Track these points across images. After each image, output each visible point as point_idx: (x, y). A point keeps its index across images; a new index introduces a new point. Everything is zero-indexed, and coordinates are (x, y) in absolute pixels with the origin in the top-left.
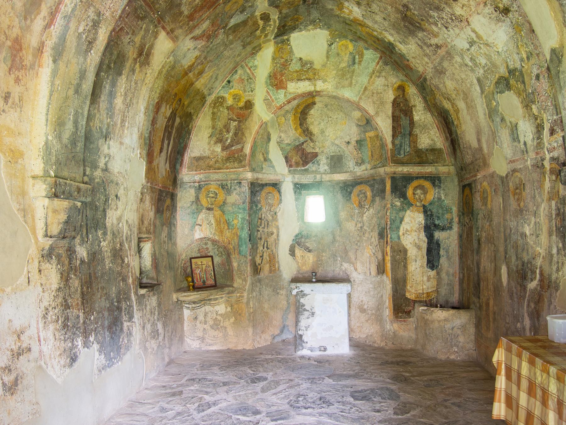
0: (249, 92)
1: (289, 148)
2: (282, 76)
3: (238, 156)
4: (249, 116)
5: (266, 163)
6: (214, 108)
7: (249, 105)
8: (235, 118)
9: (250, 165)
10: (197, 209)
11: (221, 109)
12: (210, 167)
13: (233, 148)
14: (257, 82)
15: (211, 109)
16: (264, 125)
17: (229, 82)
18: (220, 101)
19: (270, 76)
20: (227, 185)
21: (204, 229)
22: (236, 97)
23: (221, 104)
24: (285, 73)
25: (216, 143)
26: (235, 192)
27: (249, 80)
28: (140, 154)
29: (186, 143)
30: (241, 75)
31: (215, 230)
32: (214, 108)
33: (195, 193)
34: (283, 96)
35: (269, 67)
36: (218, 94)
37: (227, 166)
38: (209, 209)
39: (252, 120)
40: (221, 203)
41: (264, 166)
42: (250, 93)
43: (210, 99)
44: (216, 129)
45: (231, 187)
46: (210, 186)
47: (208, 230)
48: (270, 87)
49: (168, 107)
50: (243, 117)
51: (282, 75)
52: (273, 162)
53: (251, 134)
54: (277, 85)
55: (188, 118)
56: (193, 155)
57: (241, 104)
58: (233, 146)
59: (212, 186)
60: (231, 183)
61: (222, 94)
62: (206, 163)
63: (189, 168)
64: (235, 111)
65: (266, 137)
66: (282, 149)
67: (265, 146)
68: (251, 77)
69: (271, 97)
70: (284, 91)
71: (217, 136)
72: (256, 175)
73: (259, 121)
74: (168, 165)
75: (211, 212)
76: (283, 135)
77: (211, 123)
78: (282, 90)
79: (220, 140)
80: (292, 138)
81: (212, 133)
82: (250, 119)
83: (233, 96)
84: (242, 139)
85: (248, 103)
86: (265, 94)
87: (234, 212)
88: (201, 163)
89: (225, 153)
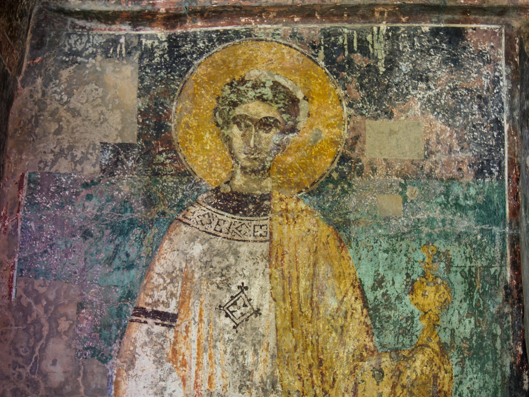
10: (149, 202)
20: (364, 48)
21: (189, 350)
26: (419, 95)
31: (279, 356)
33: (144, 91)
38: (234, 202)
40: (325, 164)
45: (391, 63)
46: (244, 49)
47: (222, 353)
59: (263, 52)
60: (393, 36)
72: (172, 32)
75: (252, 225)
87: (416, 228)
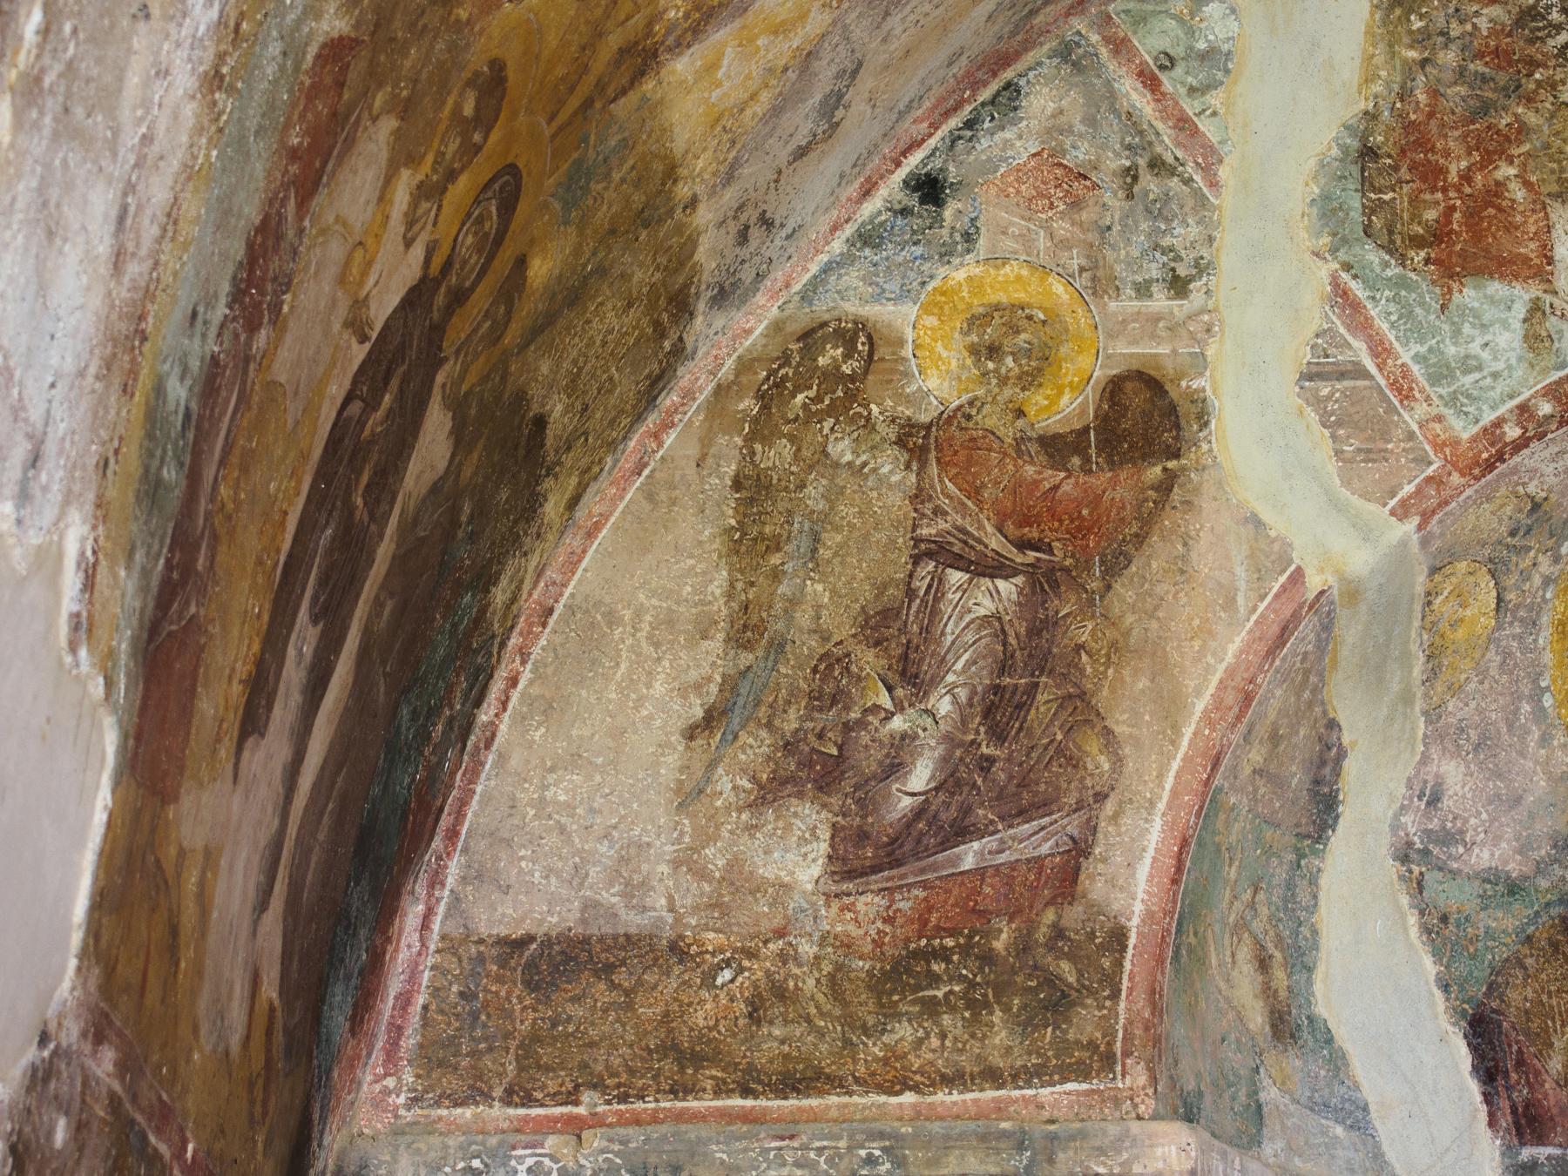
0: (1143, 290)
1: (1507, 921)
2: (1488, 160)
3: (1023, 946)
4: (1147, 523)
5: (1293, 1062)
6: (760, 431)
7: (1146, 421)
8: (995, 542)
9: (1157, 1049)
11: (842, 450)
12: (683, 1060)
13: (969, 855)
14: (1227, 201)
15: (729, 447)
16: (1307, 628)
17: (930, 189)
18: (829, 369)
19: (1368, 153)
22: (1006, 340)
23: (845, 398)
24: (1523, 130)
25: (769, 793)
27: (1150, 184)
28: (89, 584)
29: (434, 771)
30: (1056, 129)
32: (760, 431)
34: (1509, 339)
35: (1349, 71)
36: (806, 296)
37: (893, 1056)
39: (1182, 569)
41: (1270, 1094)
42: (1160, 301)
43: (726, 341)
44: (779, 647)
48: (1373, 256)
49: (401, 197)
50: (1080, 530)
51: (1493, 147)
52: (1360, 1066)
53: (1171, 709)
54: (1438, 235)
55: (517, 469)
56: (499, 917)
57: (1065, 404)
58: (962, 832)
61: (852, 298)
62: (648, 1011)
63: (434, 1058)
64: (997, 476)
65: (1297, 777)
66: (1439, 928)
67: (1281, 874)
68: (1168, 144)
69: (1380, 351)
70: (1522, 295)
71: (790, 722)
73: (1260, 575)
74: (273, 921)
76: (1453, 772)
77: (717, 586)
78: (1496, 288)
79: (817, 767)
80: (1543, 827)
81: (730, 685)
82: (1156, 557)
83: (976, 321)
84: (1074, 763)
85: (1137, 399)
86: (1314, 313)
88: (586, 1006)
89: (869, 904)
